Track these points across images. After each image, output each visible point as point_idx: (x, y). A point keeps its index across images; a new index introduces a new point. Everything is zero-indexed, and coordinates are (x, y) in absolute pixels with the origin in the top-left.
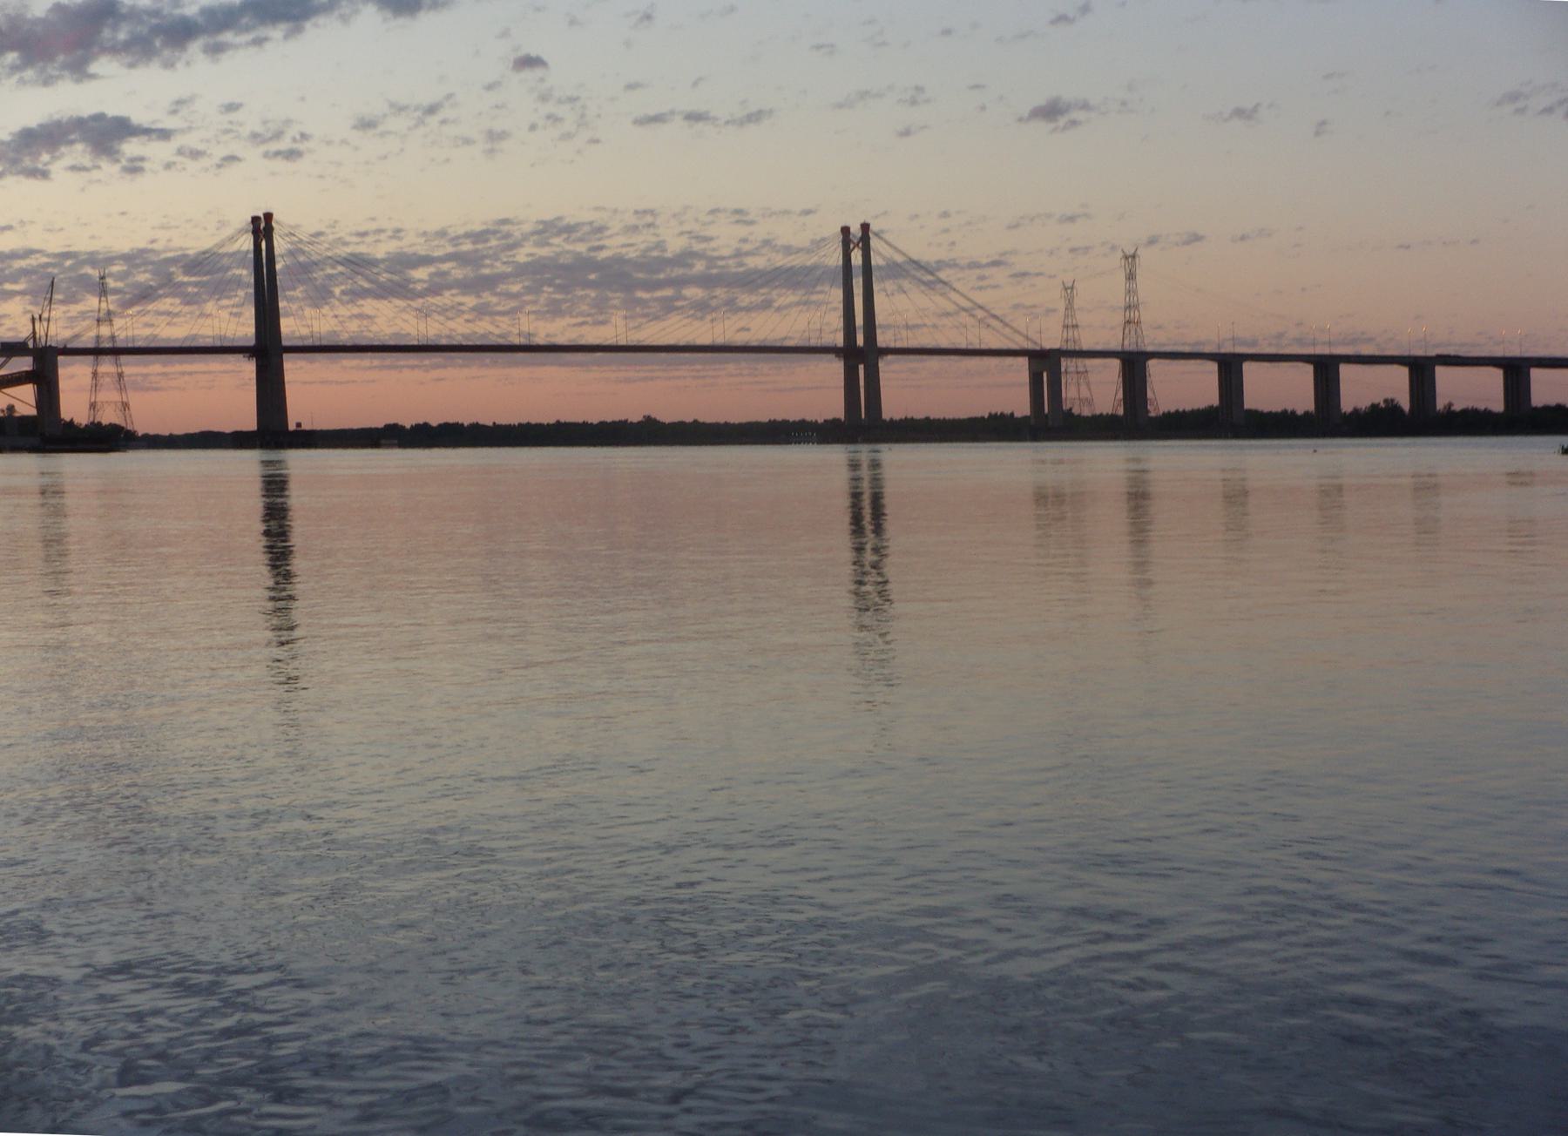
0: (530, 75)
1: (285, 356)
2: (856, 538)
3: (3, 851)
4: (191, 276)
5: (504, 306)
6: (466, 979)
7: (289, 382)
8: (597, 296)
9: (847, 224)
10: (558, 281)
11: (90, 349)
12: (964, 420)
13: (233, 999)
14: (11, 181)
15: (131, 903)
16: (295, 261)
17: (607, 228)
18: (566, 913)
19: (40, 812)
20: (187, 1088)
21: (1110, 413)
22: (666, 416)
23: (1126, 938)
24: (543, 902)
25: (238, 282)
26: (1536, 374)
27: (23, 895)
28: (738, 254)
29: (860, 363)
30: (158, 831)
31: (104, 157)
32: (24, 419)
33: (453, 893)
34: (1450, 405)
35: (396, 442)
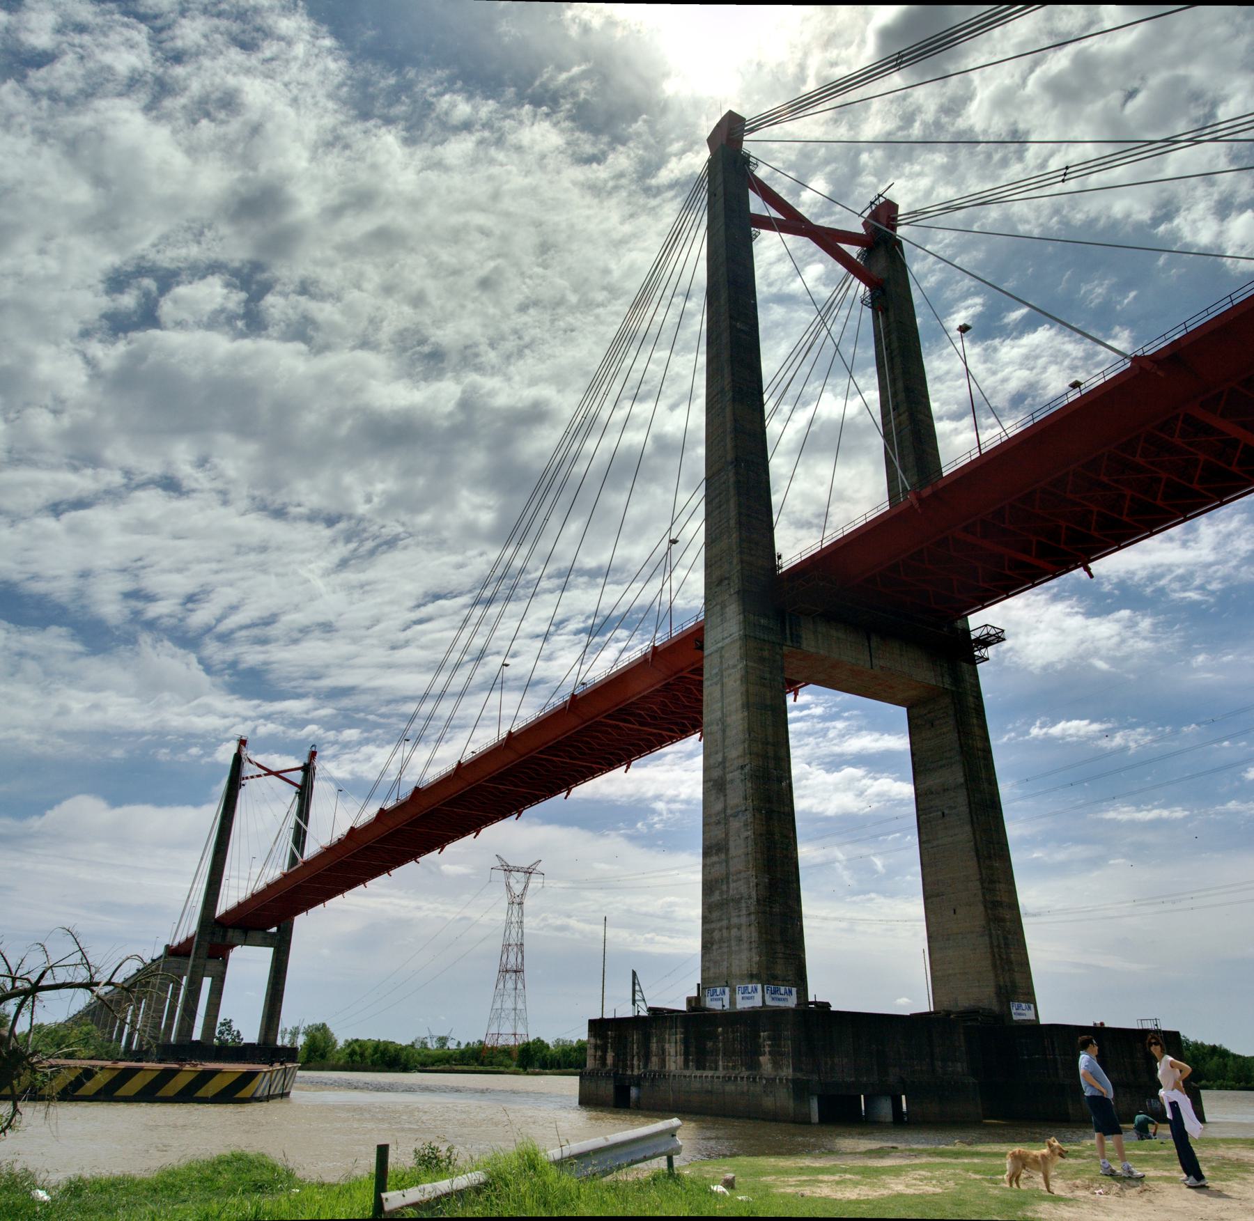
0: (957, 911)
1: (11, 1103)
2: (672, 912)
3: (1250, 1125)
4: (1114, 819)
5: (907, 1186)
6: (96, 111)
7: (939, 379)
8: (579, 301)
9: (318, 1021)
10: (194, 751)
11: (386, 1162)
12: (144, 1102)
13: (1115, 97)
14: (1247, 1053)
15: (143, 567)
16: (996, 1007)
17: (826, 122)
18: (464, 552)
19: (303, 300)
20: (484, 375)
21: (1008, 342)
22: (402, 1037)
23: (175, 995)
24: (869, 639)
25: (935, 401)
26: (267, 953)
27: (719, 607)
28: (595, 1060)
29: (197, 1042)
30: (1078, 1182)
31: (862, 126)
32: (644, 1017)
33: (735, 562)
34: (468, 1044)
35: (1069, 739)
